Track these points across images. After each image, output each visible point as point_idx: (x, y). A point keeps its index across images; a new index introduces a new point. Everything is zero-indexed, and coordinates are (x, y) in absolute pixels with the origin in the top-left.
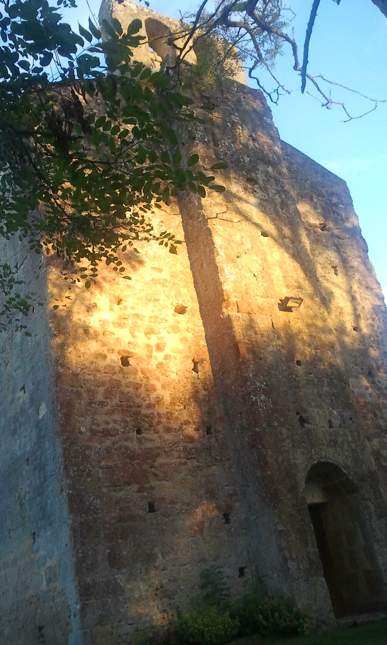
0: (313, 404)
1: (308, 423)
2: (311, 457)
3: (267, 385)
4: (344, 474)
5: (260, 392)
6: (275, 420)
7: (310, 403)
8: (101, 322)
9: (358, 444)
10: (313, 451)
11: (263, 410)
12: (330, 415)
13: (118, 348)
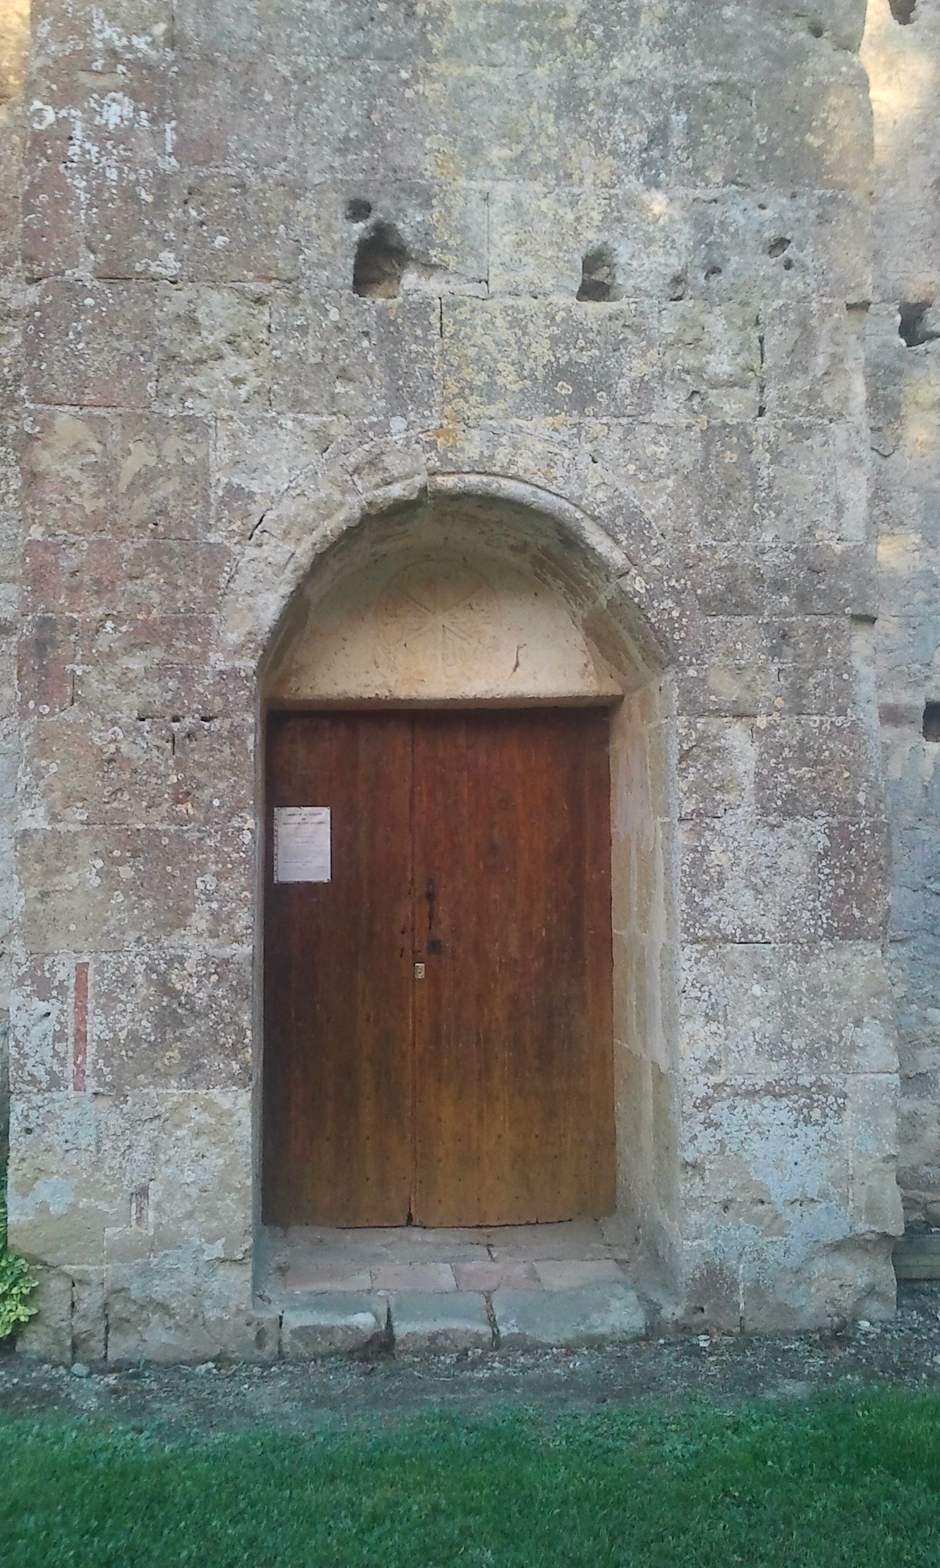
0: (497, 153)
1: (429, 268)
2: (374, 462)
3: (173, 40)
4: (602, 566)
5: (104, 81)
6: (167, 244)
7: (475, 148)
8: (918, 1216)
9: (771, 394)
10: (397, 424)
11: (97, 193)
12: (612, 220)
13: (723, 932)
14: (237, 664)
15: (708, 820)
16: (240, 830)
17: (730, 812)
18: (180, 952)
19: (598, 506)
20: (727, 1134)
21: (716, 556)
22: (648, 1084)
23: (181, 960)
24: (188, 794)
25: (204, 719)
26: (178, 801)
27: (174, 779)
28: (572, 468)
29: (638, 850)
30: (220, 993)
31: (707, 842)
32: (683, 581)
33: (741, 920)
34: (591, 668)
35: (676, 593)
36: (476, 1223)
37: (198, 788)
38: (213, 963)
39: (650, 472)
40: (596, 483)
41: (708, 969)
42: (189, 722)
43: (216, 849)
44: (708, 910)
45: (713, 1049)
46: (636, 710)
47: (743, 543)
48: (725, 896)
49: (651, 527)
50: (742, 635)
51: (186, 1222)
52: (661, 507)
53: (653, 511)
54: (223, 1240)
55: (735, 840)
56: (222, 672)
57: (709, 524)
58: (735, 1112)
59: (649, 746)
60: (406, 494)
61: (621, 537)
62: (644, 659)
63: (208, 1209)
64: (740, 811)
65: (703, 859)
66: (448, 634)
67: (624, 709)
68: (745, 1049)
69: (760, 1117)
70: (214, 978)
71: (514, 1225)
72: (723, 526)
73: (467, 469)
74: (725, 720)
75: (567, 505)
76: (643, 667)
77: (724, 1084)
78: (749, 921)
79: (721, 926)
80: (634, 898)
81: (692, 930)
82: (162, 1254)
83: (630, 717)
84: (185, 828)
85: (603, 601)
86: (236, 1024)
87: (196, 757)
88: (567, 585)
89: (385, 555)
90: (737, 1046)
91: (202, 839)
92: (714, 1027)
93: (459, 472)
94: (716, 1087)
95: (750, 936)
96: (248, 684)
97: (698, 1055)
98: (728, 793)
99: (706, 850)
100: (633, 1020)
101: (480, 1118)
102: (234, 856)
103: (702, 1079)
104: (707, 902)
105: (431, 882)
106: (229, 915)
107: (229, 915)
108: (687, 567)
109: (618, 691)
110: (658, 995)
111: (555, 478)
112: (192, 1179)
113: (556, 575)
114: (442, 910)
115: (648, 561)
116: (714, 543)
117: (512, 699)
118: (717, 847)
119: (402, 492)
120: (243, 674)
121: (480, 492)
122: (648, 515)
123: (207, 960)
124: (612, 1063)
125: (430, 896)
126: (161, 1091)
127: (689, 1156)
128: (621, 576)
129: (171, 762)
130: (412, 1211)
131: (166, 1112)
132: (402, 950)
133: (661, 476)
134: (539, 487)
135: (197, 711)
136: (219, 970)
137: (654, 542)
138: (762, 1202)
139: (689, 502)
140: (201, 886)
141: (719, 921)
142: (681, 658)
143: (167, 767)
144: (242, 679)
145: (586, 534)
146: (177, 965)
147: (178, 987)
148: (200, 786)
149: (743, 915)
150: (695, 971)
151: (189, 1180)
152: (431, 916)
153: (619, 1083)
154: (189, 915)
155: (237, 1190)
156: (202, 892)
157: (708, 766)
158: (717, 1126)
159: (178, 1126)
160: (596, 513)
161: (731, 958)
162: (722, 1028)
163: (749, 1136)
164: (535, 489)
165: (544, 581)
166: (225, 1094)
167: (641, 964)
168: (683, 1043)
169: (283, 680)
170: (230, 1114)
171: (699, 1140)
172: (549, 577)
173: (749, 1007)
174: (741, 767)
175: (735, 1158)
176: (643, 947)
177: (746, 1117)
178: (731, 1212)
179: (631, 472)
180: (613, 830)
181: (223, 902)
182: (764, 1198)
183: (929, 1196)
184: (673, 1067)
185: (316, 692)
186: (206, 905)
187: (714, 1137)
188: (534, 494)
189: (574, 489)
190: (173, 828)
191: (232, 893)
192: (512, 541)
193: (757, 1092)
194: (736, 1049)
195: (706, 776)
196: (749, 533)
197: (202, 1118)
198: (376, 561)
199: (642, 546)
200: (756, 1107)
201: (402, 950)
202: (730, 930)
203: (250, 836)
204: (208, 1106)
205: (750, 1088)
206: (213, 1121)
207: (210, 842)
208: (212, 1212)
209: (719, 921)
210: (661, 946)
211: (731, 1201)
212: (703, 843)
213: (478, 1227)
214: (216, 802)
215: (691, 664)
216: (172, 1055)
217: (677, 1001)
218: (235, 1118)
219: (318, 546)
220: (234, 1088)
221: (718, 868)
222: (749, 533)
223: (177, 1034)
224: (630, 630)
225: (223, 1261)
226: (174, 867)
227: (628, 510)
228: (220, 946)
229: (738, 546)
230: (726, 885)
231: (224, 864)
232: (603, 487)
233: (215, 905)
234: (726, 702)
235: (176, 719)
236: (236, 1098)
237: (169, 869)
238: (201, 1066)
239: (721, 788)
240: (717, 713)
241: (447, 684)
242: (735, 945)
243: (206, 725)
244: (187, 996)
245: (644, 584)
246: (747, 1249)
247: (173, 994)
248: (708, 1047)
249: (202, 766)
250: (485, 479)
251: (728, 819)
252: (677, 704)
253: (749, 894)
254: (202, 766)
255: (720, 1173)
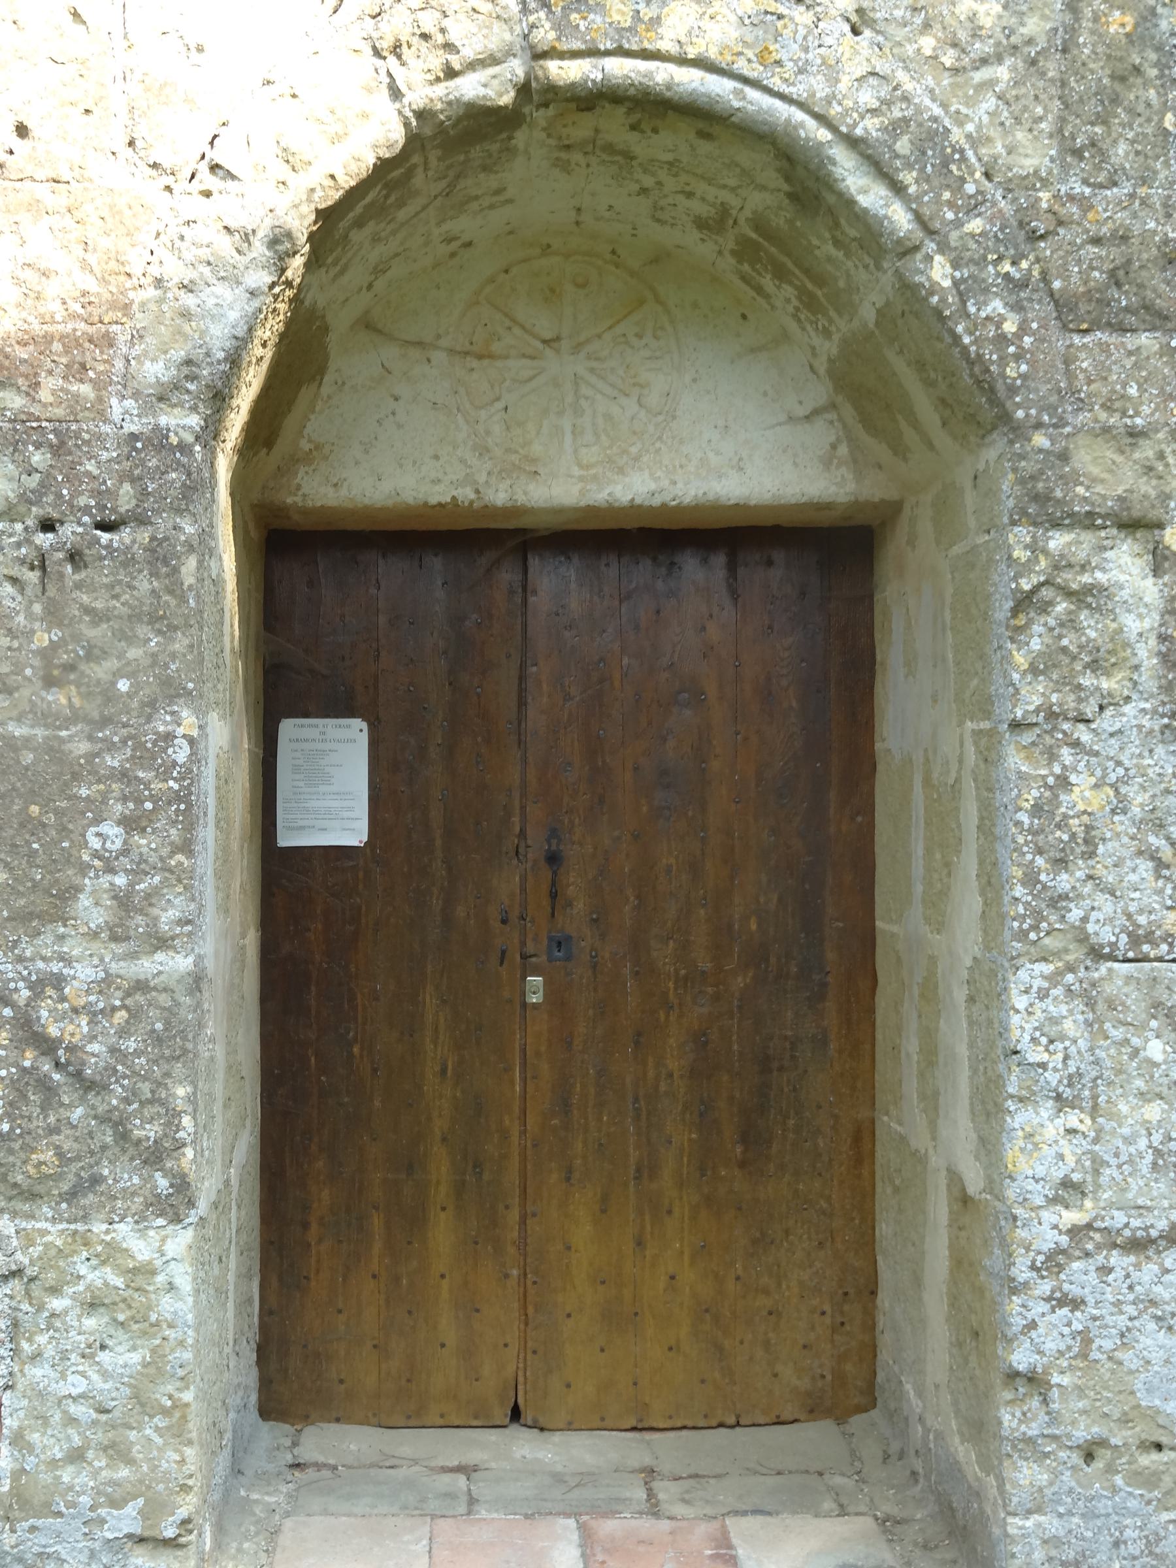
14: (163, 420)
15: (1066, 726)
16: (169, 737)
17: (1109, 712)
18: (55, 967)
19: (863, 118)
20: (1095, 1319)
21: (1090, 215)
22: (940, 1209)
23: (58, 982)
24: (70, 667)
25: (106, 526)
26: (50, 682)
27: (42, 639)
28: (812, 42)
29: (927, 781)
30: (131, 1045)
31: (1064, 767)
32: (1024, 265)
33: (1129, 916)
34: (843, 450)
35: (1014, 285)
36: (633, 1422)
37: (89, 657)
38: (118, 988)
39: (963, 51)
40: (858, 74)
41: (1064, 1009)
42: (69, 531)
43: (124, 775)
44: (1065, 897)
45: (1071, 1160)
46: (925, 527)
47: (1142, 191)
48: (1100, 870)
49: (964, 159)
50: (1140, 369)
51: (71, 1469)
52: (986, 119)
53: (970, 127)
54: (141, 1501)
55: (1119, 763)
56: (134, 437)
57: (1078, 153)
58: (1110, 1278)
59: (949, 591)
60: (491, 93)
61: (908, 177)
62: (944, 424)
63: (113, 1445)
64: (1128, 709)
65: (1055, 801)
66: (584, 390)
67: (907, 511)
68: (1130, 1162)
69: (1158, 1289)
70: (121, 1016)
71: (694, 1428)
72: (1104, 156)
73: (609, 45)
74: (1103, 534)
75: (799, 116)
76: (942, 439)
77: (1089, 1226)
78: (1142, 920)
79: (1091, 928)
80: (918, 867)
81: (1033, 936)
82: (26, 1525)
83: (911, 542)
84: (64, 733)
85: (868, 314)
86: (163, 1103)
87: (85, 598)
88: (802, 292)
89: (469, 244)
90: (1117, 1155)
91: (97, 755)
92: (1073, 1119)
93: (593, 52)
94: (1074, 1232)
95: (1146, 948)
96: (184, 460)
97: (1040, 1171)
98: (1108, 675)
99: (1064, 783)
100: (911, 1087)
101: (640, 1243)
102: (156, 786)
103: (1048, 1216)
104: (1064, 882)
105: (554, 833)
106: (150, 897)
107: (150, 897)
108: (1034, 237)
109: (892, 494)
110: (963, 1050)
111: (778, 63)
112: (80, 1390)
113: (781, 274)
114: (575, 884)
115: (958, 224)
116: (1087, 191)
117: (696, 509)
118: (1082, 781)
119: (482, 91)
120: (174, 440)
121: (632, 91)
122: (957, 135)
123: (107, 983)
124: (872, 1153)
125: (553, 859)
126: (24, 1224)
127: (1021, 1358)
128: (904, 254)
129: (37, 608)
130: (521, 1401)
131: (32, 1263)
132: (503, 952)
133: (984, 61)
134: (746, 80)
135: (86, 510)
136: (127, 1002)
137: (970, 188)
138: (1159, 1447)
139: (1039, 110)
140: (95, 843)
141: (1085, 920)
142: (1020, 414)
143: (30, 616)
144: (172, 449)
145: (838, 172)
146: (49, 991)
147: (53, 1031)
148: (93, 654)
149: (1132, 908)
150: (1039, 1013)
151: (75, 1392)
152: (553, 896)
153: (883, 1192)
154: (75, 898)
155: (166, 1412)
156: (96, 855)
157: (1070, 623)
158: (1076, 1304)
159: (55, 1291)
160: (859, 131)
161: (1109, 989)
162: (1088, 1121)
163: (1137, 1323)
164: (739, 86)
165: (759, 290)
166: (142, 1233)
167: (930, 992)
168: (1014, 1154)
169: (285, 470)
170: (148, 1270)
171: (1041, 1330)
172: (767, 282)
173: (1139, 1083)
174: (1132, 624)
175: (1109, 1365)
176: (933, 960)
177: (1131, 1288)
178: (1099, 1464)
179: (928, 52)
180: (878, 746)
181: (138, 873)
182: (1164, 1440)
183: (332, 273)
184: (993, 1186)
185: (344, 492)
186: (105, 881)
187: (1069, 1324)
188: (736, 92)
189: (815, 86)
190: (40, 733)
191: (153, 859)
192: (703, 210)
193: (1153, 1241)
194: (1113, 1162)
195: (1065, 642)
196: (1155, 172)
197: (93, 1276)
198: (453, 255)
199: (947, 195)
200: (1152, 1268)
201: (503, 952)
202: (1106, 935)
203: (187, 749)
204: (112, 1254)
205: (1139, 1233)
206: (119, 1282)
207: (112, 761)
208: (117, 1452)
209: (1085, 920)
210: (968, 962)
211: (1103, 1443)
212: (1057, 770)
213: (634, 1429)
214: (123, 685)
215: (1039, 425)
216: (42, 1157)
217: (1001, 1067)
218: (160, 1279)
219: (319, 193)
220: (160, 1222)
221: (1085, 818)
222: (1155, 172)
223: (52, 1119)
224: (920, 366)
225: (141, 1540)
226: (45, 807)
227: (920, 125)
228: (133, 956)
229: (1132, 196)
230: (1101, 849)
231: (139, 801)
232: (873, 81)
233: (121, 880)
234: (1104, 497)
235: (48, 526)
236: (163, 1240)
237: (34, 810)
238: (96, 1180)
239: (1094, 666)
240: (1088, 521)
241: (581, 479)
242: (1116, 965)
243: (105, 537)
244: (71, 1049)
245: (948, 270)
246: (1129, 1533)
247: (46, 1046)
248: (1061, 1157)
249: (97, 617)
250: (642, 65)
251: (1107, 722)
252: (1011, 503)
253: (1145, 867)
254: (97, 617)
255: (1080, 1391)
